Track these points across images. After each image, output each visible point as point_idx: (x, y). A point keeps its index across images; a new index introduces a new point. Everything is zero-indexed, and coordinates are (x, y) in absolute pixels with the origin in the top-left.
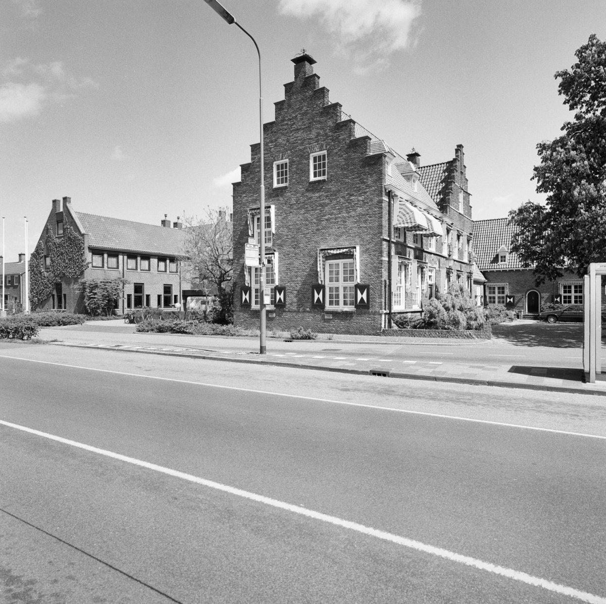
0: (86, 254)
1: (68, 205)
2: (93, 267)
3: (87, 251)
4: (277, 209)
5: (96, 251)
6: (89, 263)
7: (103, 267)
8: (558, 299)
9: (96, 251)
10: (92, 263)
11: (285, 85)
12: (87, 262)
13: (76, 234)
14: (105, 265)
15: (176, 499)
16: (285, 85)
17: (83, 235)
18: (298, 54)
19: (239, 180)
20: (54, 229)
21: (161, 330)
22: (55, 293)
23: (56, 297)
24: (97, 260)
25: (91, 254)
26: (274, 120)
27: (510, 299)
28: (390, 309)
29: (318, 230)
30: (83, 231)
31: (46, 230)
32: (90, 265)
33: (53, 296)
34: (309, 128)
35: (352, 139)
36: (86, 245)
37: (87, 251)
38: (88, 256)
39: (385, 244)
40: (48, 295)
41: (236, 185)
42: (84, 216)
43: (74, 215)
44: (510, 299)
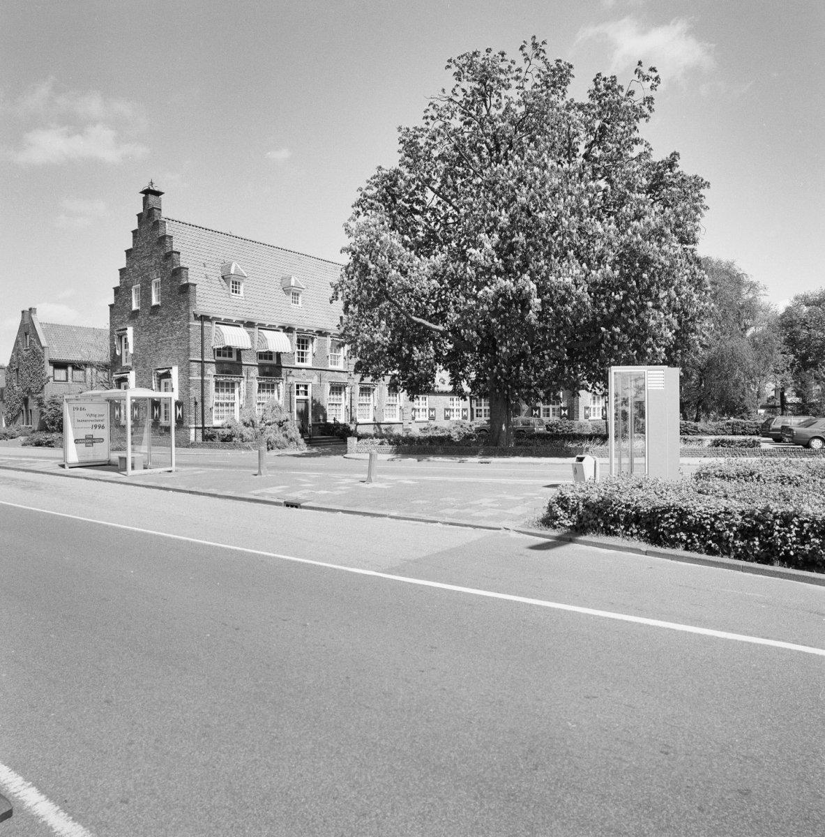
0: (46, 369)
1: (33, 316)
2: (54, 381)
3: (47, 364)
4: (135, 330)
5: (59, 365)
6: (49, 377)
7: (67, 380)
8: (537, 412)
9: (59, 365)
10: (54, 377)
11: (138, 215)
12: (47, 376)
13: (38, 347)
14: (70, 378)
15: (423, 671)
16: (138, 215)
17: (43, 348)
18: (145, 186)
19: (113, 302)
20: (23, 342)
21: (39, 444)
22: (24, 408)
23: (25, 412)
24: (61, 374)
25: (52, 367)
26: (132, 247)
27: (536, 414)
28: (203, 423)
29: (156, 351)
30: (44, 343)
31: (17, 342)
32: (51, 379)
33: (23, 411)
34: (150, 257)
35: (174, 268)
36: (46, 358)
37: (47, 364)
38: (49, 369)
39: (195, 366)
40: (18, 411)
41: (111, 306)
42: (51, 328)
43: (38, 327)
44: (536, 414)
